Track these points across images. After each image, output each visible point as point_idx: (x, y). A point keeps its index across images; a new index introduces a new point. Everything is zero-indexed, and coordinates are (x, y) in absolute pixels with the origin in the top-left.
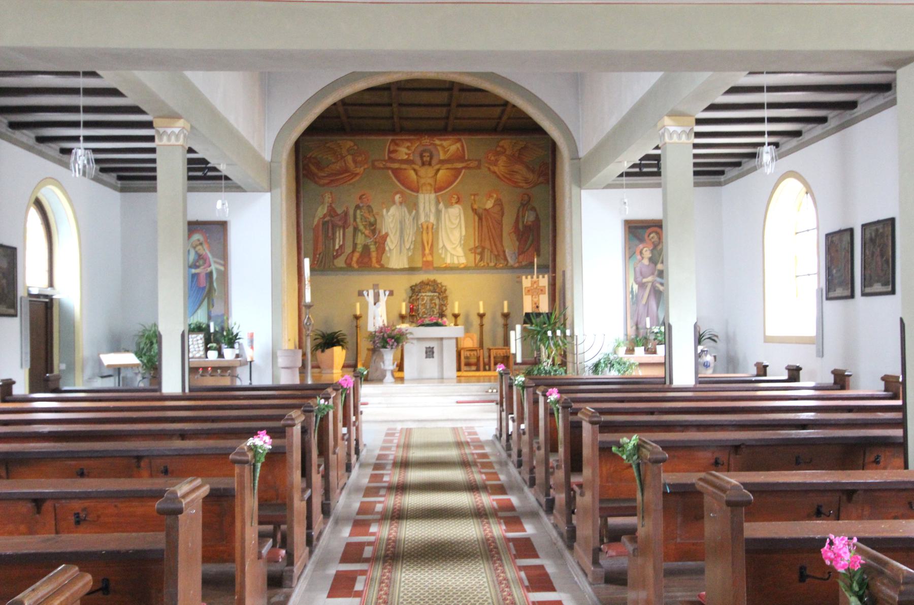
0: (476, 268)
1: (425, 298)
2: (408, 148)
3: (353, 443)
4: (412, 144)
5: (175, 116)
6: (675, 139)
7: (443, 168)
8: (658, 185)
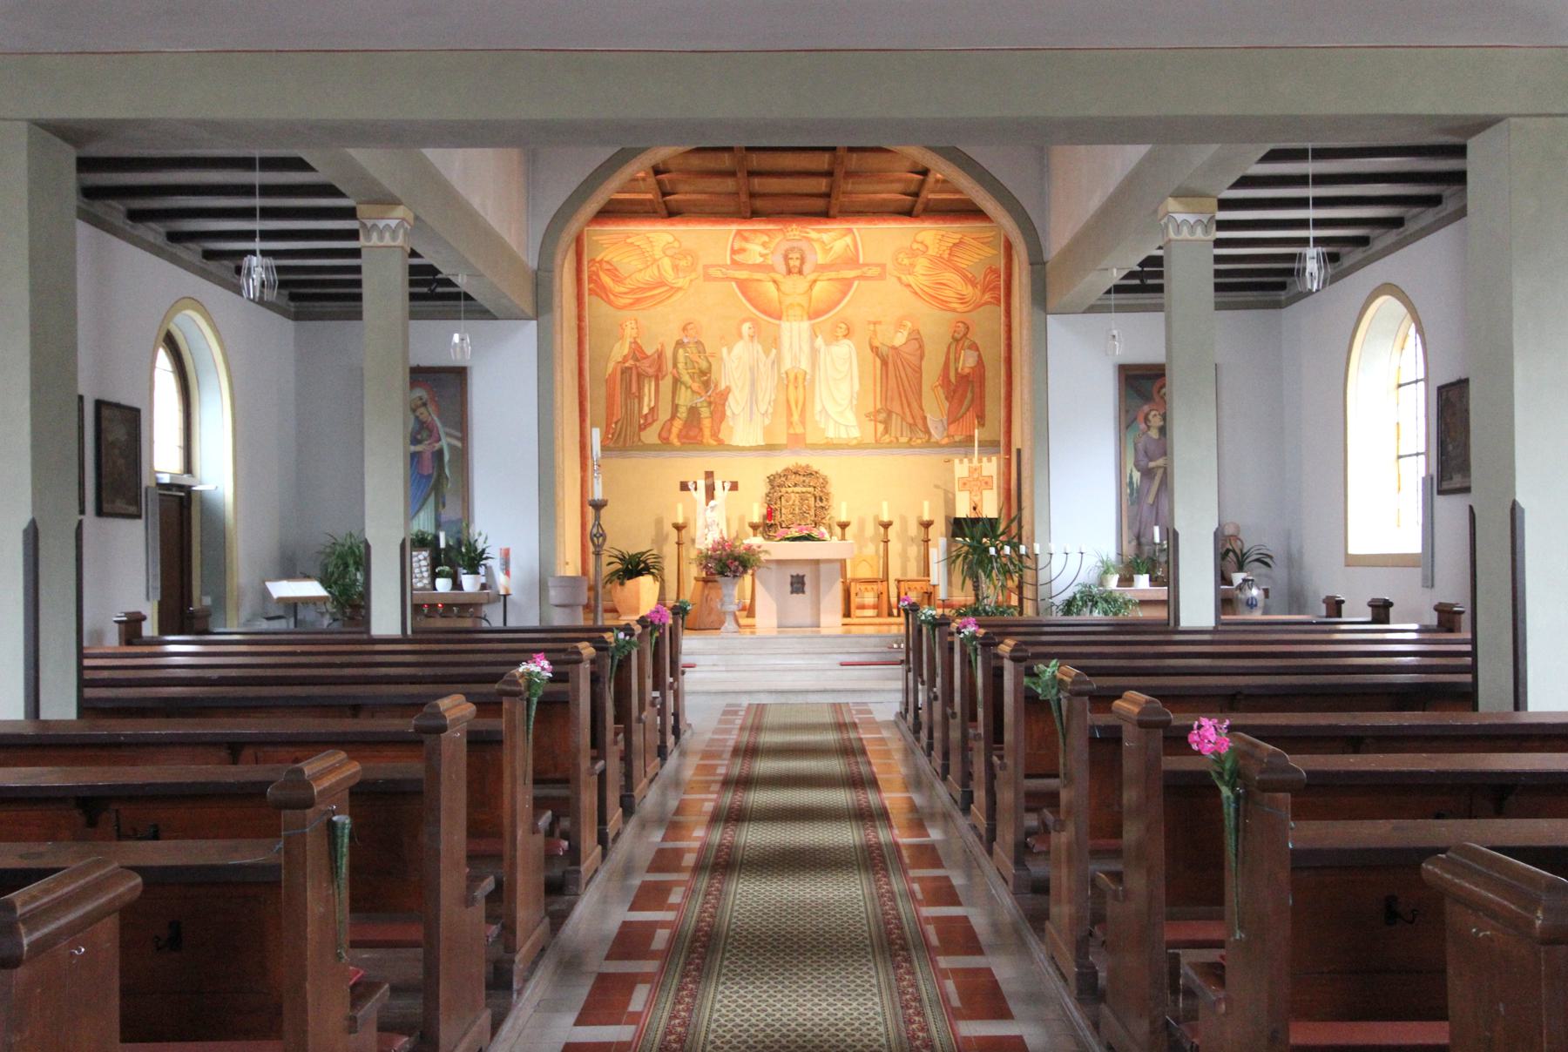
0: (878, 445)
2: (764, 245)
3: (671, 720)
4: (769, 236)
5: (391, 201)
6: (1185, 233)
8: (1159, 308)
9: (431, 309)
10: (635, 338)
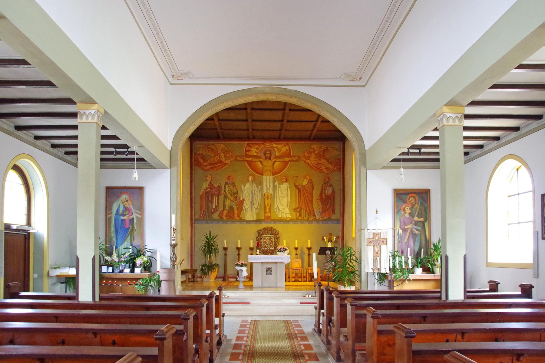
0: (297, 220)
1: (266, 237)
2: (257, 149)
4: (259, 146)
6: (451, 122)
7: (277, 161)
9: (130, 164)
10: (211, 181)
